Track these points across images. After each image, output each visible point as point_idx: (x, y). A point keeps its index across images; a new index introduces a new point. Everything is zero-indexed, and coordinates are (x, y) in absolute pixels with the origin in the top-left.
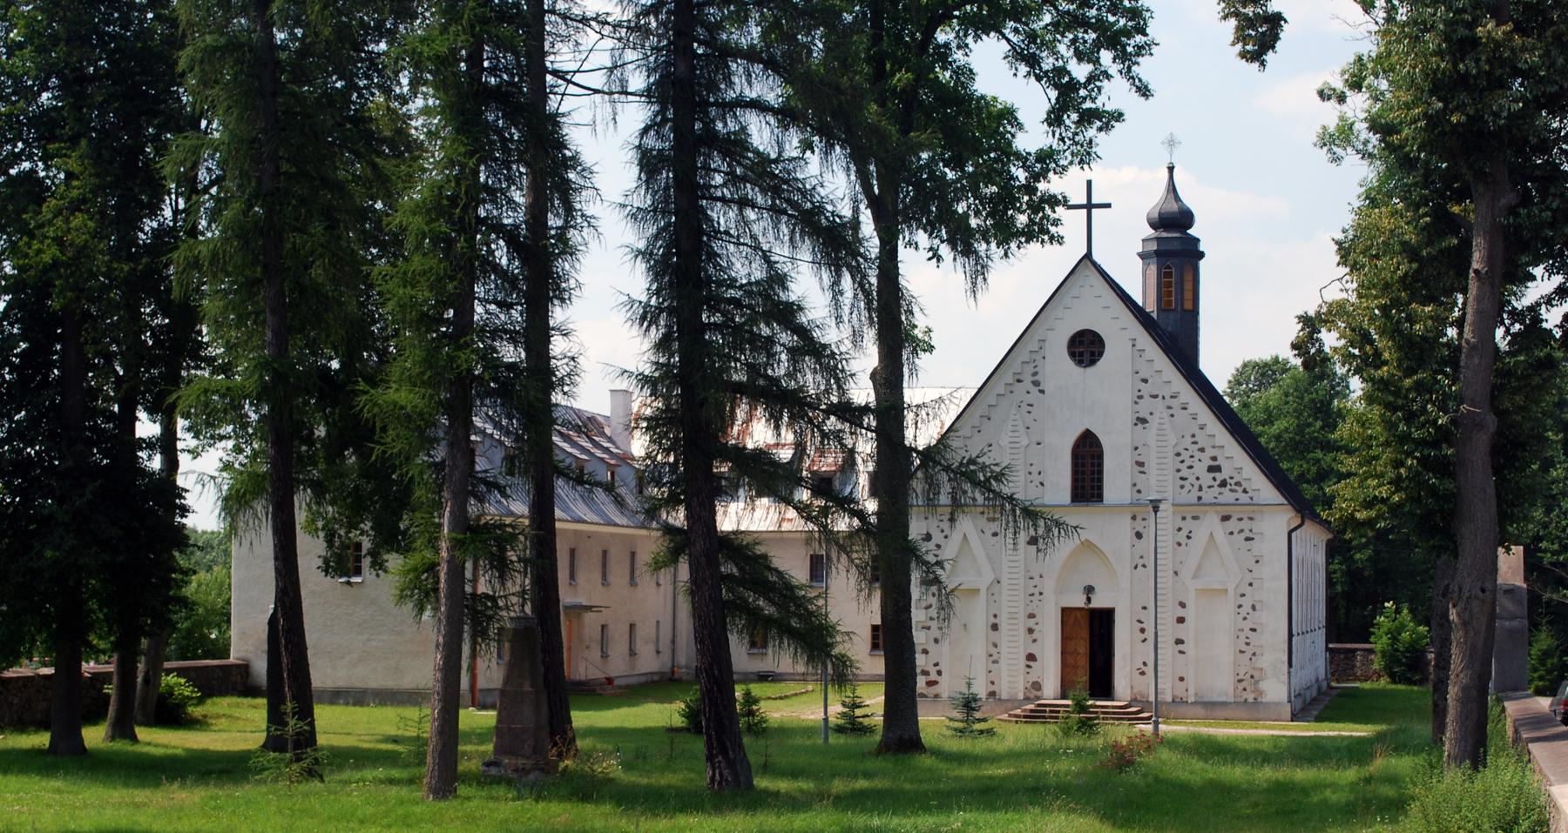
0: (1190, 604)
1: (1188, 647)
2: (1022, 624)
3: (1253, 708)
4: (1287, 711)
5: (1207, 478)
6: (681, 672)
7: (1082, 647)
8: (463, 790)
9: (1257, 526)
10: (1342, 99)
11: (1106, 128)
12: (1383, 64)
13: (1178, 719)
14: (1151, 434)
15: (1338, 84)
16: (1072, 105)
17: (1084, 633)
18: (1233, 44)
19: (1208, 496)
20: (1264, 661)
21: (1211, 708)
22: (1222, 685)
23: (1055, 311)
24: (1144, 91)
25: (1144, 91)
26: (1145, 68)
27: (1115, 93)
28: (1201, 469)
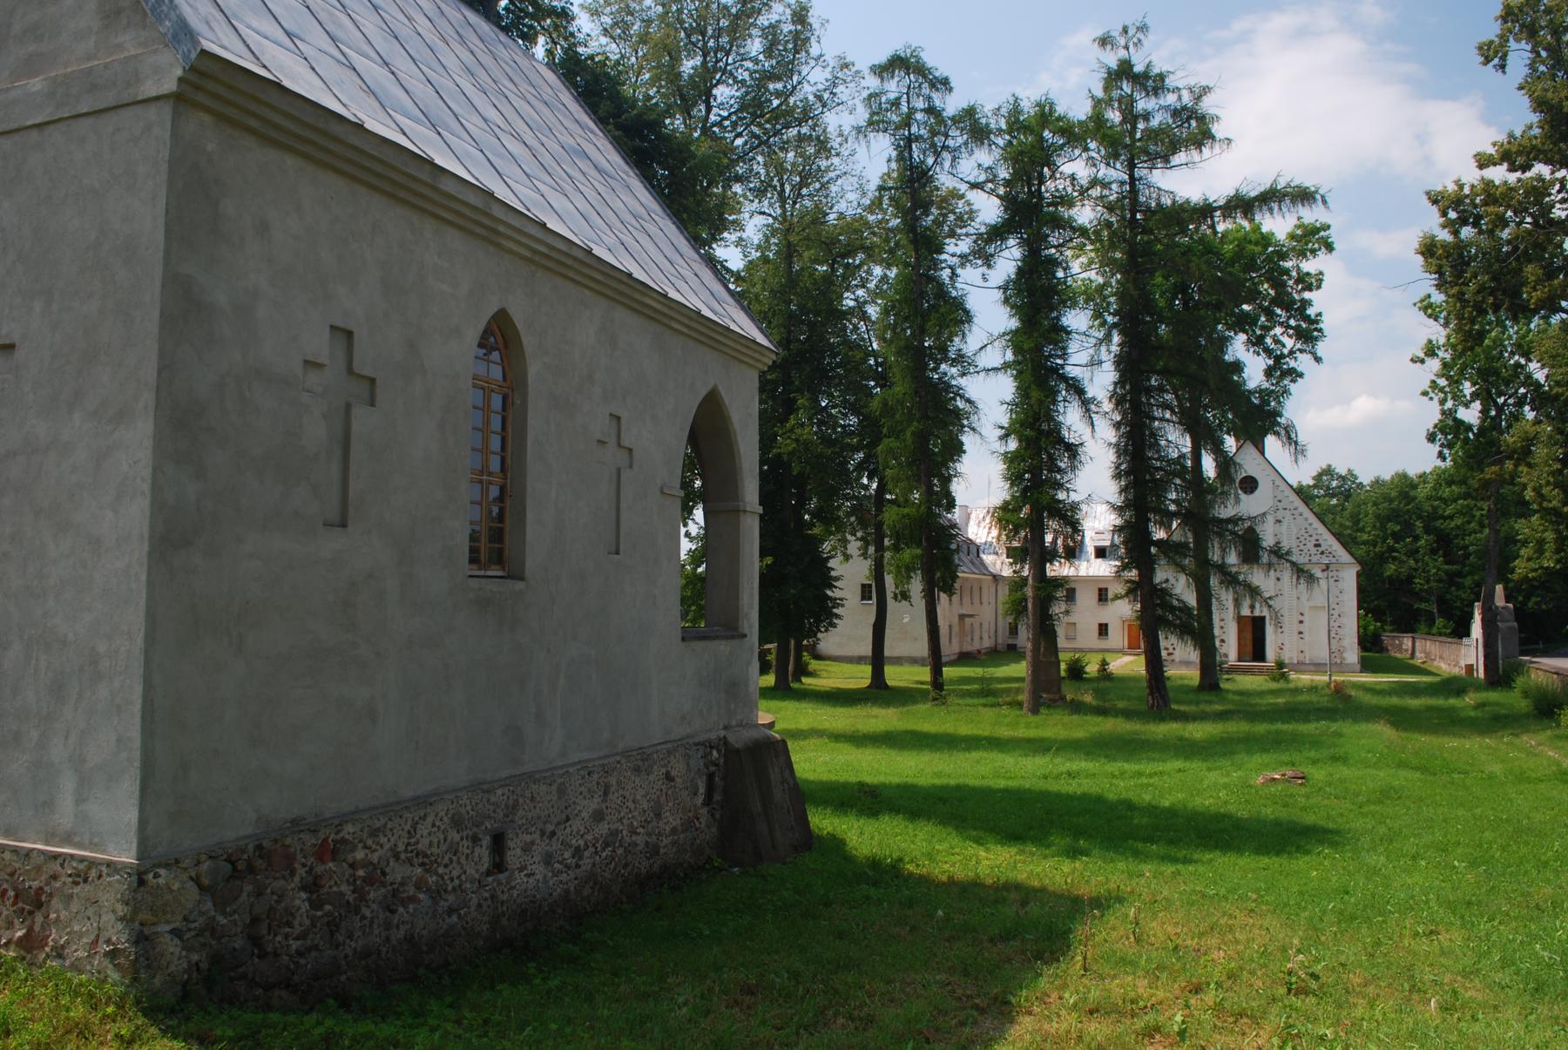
0: (1306, 613)
1: (1306, 636)
2: (1296, 627)
3: (1341, 667)
4: (1358, 667)
5: (1314, 550)
6: (1000, 647)
7: (1249, 636)
8: (950, 700)
9: (1341, 574)
10: (1422, 361)
11: (1293, 381)
12: (1174, 202)
13: (1303, 672)
14: (1284, 528)
15: (1422, 355)
16: (1281, 371)
17: (1250, 629)
18: (1320, 314)
19: (1314, 559)
20: (1346, 643)
21: (1317, 667)
22: (1322, 654)
23: (1269, 470)
24: (1318, 360)
25: (1318, 360)
26: (1321, 349)
27: (1303, 362)
28: (1310, 546)
